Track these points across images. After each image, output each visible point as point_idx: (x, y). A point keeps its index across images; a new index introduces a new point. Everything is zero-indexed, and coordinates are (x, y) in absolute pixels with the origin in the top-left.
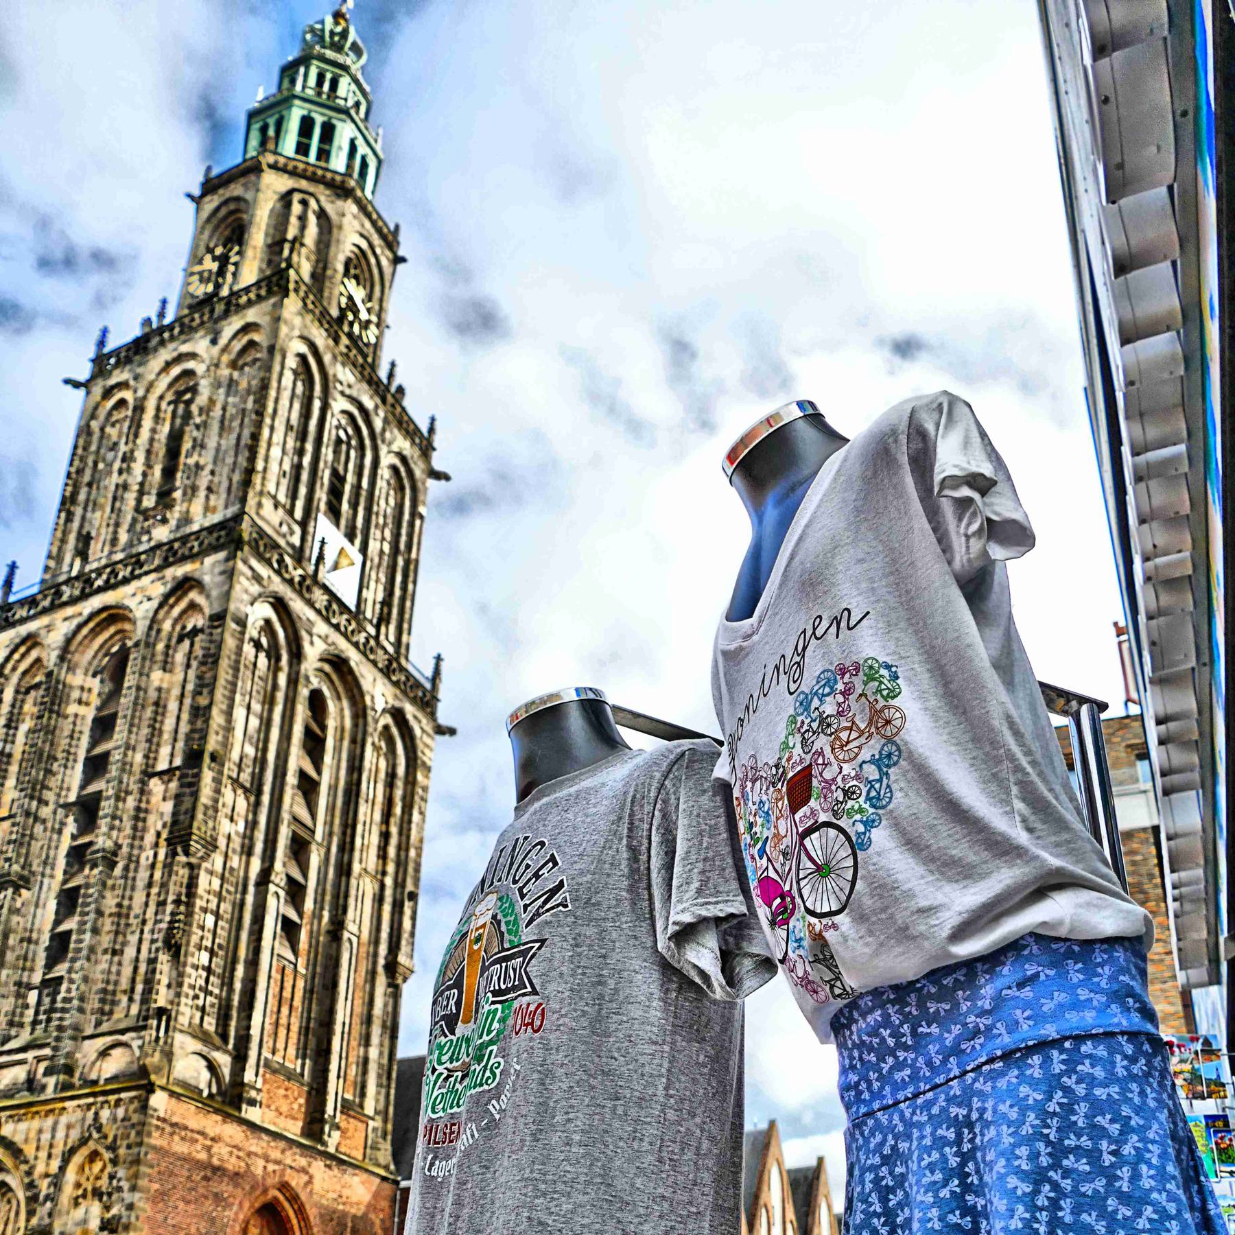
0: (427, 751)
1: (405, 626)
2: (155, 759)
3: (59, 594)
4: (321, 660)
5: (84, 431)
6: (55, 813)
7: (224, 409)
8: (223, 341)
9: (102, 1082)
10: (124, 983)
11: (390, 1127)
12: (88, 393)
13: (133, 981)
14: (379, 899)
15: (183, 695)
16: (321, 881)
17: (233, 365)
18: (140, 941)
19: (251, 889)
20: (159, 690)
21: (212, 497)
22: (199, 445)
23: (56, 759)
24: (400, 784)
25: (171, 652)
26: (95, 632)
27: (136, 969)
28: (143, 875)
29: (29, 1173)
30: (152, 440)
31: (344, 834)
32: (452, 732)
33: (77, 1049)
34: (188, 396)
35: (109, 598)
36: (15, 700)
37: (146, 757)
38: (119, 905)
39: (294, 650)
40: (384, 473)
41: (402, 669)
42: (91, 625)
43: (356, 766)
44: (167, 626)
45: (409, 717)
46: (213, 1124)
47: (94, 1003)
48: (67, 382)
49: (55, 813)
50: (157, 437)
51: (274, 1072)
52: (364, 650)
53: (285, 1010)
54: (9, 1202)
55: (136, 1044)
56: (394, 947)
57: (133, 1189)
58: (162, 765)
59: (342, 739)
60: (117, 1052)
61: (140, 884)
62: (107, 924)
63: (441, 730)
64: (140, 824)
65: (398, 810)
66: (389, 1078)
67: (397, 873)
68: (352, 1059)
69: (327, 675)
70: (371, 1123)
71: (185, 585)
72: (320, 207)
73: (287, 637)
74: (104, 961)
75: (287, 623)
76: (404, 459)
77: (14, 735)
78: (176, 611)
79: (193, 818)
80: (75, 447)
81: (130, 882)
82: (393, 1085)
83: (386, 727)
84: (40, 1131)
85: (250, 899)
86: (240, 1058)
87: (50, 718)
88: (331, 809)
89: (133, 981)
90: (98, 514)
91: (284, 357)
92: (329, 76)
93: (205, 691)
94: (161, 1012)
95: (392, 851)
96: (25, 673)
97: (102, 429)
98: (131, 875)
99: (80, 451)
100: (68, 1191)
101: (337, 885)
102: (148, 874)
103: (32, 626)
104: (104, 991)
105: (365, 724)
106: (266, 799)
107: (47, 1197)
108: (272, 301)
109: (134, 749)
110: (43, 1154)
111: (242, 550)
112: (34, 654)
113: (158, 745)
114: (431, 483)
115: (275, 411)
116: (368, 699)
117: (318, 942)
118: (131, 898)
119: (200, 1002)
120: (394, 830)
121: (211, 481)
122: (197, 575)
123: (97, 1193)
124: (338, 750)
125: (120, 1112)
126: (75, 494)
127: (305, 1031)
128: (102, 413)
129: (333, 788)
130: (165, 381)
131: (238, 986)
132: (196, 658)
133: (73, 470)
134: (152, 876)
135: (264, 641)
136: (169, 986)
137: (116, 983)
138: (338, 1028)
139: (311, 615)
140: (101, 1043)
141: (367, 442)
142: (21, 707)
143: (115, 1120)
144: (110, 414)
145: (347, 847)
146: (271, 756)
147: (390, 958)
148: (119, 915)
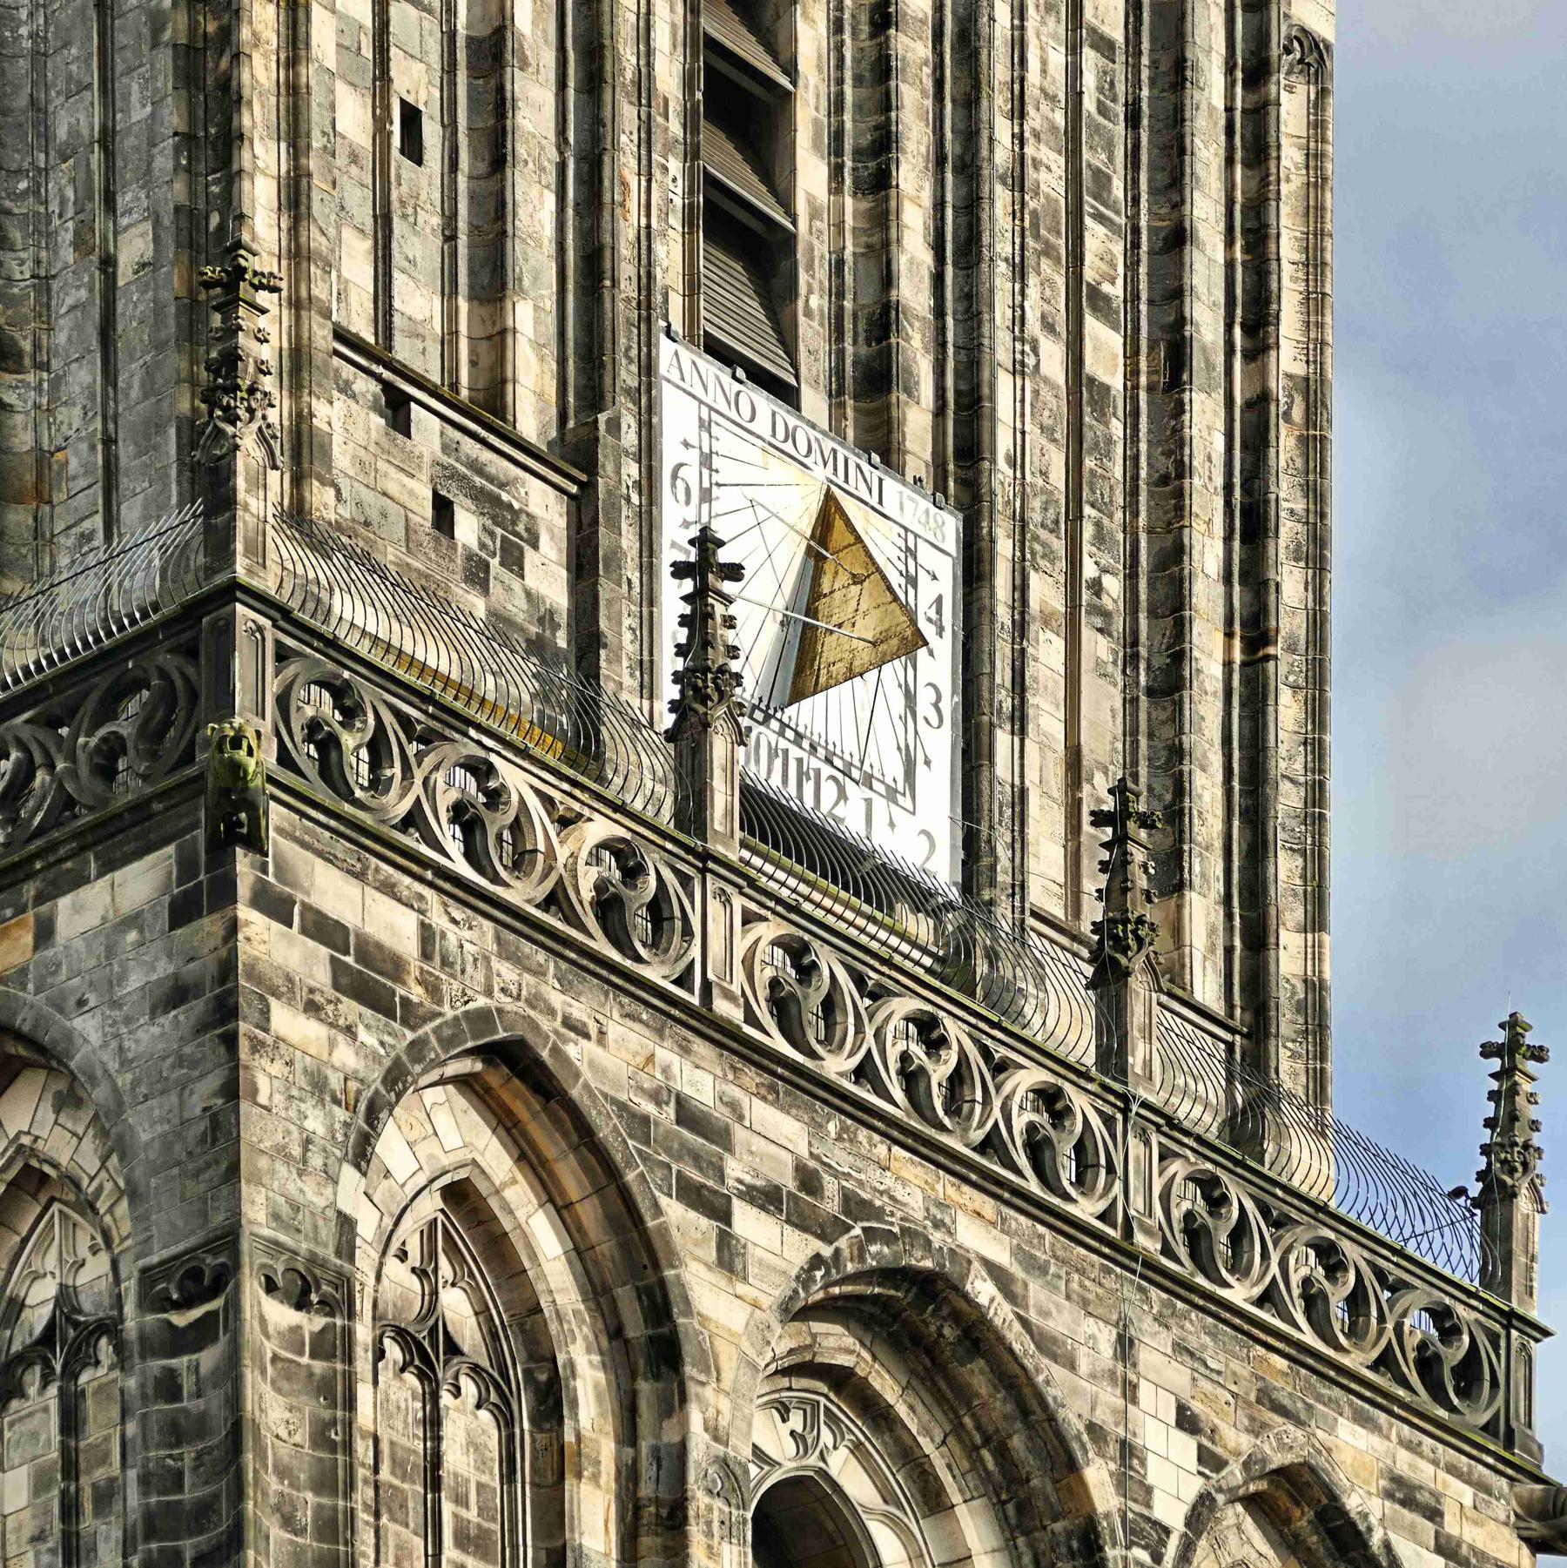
1: (1286, 868)
4: (797, 1312)
39: (635, 1328)
69: (841, 1379)
73: (580, 1252)
111: (255, 843)
116: (1098, 1476)
132: (106, 1496)
135: (456, 1307)
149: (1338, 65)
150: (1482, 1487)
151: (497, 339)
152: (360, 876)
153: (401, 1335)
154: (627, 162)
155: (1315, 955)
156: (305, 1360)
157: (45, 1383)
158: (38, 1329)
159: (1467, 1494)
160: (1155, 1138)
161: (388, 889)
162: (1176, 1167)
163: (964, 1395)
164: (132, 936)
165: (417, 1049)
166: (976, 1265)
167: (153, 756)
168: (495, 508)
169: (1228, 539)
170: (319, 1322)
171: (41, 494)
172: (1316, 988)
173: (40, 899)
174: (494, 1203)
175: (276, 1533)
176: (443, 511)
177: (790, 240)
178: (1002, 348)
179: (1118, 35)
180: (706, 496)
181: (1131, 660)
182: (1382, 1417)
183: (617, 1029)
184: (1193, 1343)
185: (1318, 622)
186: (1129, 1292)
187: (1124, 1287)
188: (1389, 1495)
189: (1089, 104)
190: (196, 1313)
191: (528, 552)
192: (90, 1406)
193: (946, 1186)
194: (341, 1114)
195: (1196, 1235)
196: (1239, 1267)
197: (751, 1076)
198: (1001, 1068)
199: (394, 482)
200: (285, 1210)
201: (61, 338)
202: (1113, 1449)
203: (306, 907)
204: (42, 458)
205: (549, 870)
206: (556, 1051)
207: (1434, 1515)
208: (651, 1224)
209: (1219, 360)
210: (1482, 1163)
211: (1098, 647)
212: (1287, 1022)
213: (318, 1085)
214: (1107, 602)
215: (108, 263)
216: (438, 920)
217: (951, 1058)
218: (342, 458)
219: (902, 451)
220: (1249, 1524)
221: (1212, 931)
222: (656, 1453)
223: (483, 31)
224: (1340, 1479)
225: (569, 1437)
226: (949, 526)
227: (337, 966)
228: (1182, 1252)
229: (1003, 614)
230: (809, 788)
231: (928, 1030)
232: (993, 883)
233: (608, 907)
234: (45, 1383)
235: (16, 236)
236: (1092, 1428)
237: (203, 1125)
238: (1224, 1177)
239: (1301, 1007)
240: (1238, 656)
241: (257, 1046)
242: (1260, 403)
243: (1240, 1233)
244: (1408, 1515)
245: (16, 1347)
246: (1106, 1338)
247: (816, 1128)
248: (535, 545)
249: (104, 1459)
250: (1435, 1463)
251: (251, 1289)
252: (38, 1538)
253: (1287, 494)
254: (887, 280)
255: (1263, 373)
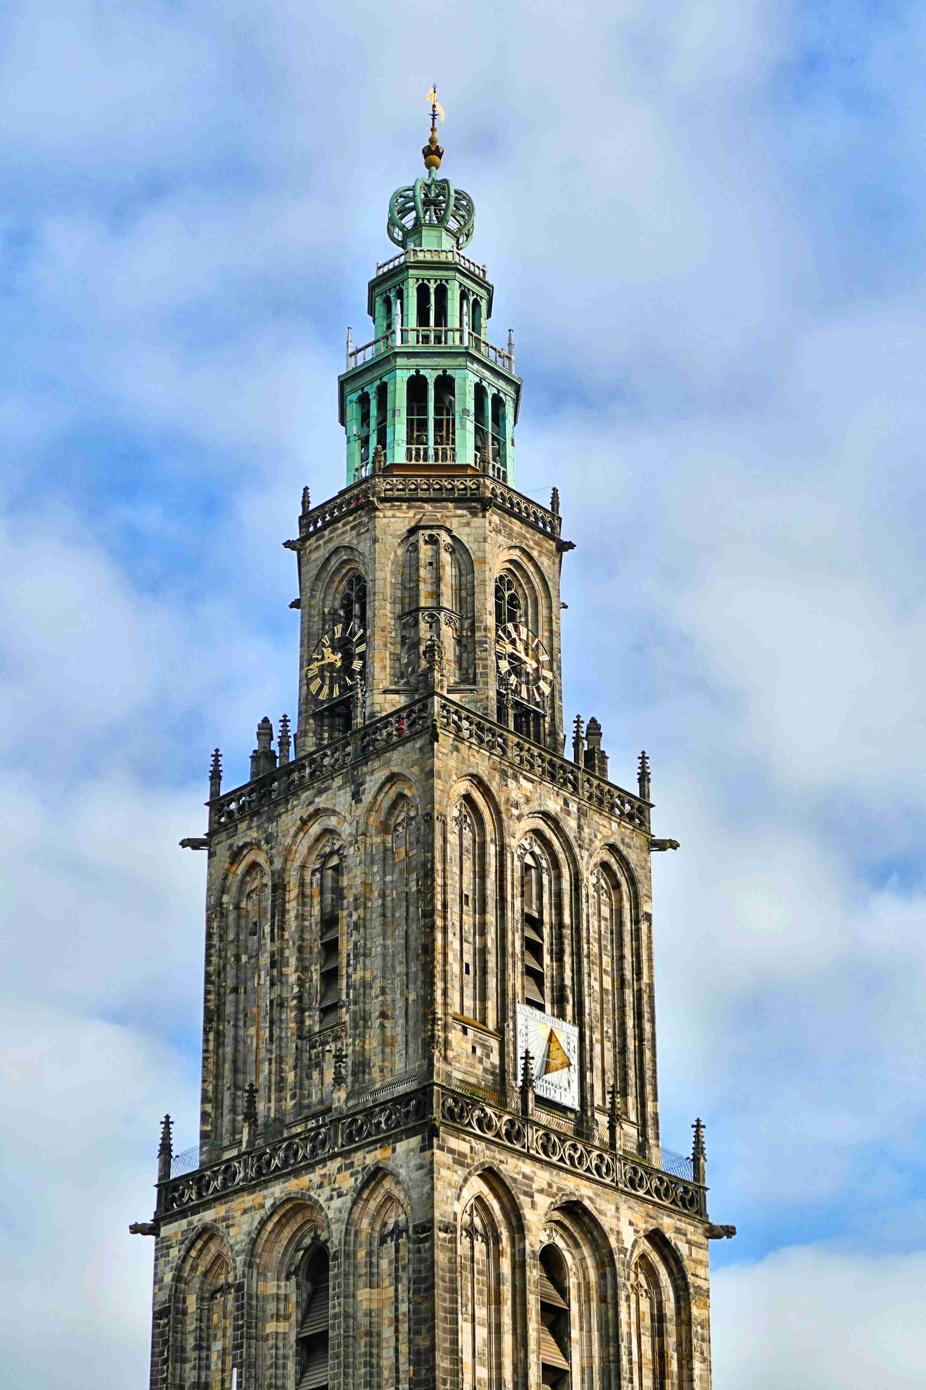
0: (701, 1271)
1: (649, 1088)
5: (215, 910)
7: (383, 896)
8: (367, 798)
12: (211, 855)
17: (385, 828)
20: (369, 1313)
21: (388, 1024)
22: (360, 953)
24: (671, 1327)
25: (374, 1260)
30: (302, 930)
32: (729, 1231)
34: (335, 861)
35: (293, 1185)
36: (201, 1309)
39: (514, 1223)
44: (365, 1224)
59: (588, 1300)
63: (713, 1233)
71: (376, 1175)
73: (503, 1208)
75: (500, 1191)
77: (208, 1358)
78: (372, 1205)
80: (209, 936)
83: (643, 1256)
87: (249, 1347)
91: (444, 824)
92: (432, 286)
93: (424, 1328)
96: (206, 1274)
97: (237, 907)
103: (209, 1216)
105: (615, 1275)
111: (438, 1136)
112: (213, 1248)
114: (656, 856)
116: (612, 1240)
121: (383, 1004)
122: (391, 1165)
124: (585, 1315)
126: (221, 1004)
130: (304, 843)
135: (477, 1221)
141: (562, 856)
142: (209, 1319)
144: (243, 882)
149: (654, 918)
150: (696, 1227)
151: (484, 1009)
152: (458, 1138)
153: (466, 1230)
154: (510, 971)
155: (655, 1107)
156: (447, 1244)
157: (392, 1241)
158: (391, 1229)
159: (692, 1229)
160: (622, 1162)
161: (464, 1140)
162: (627, 1167)
163: (584, 1223)
164: (412, 1153)
165: (470, 1174)
166: (585, 1198)
167: (417, 1115)
168: (484, 1046)
169: (634, 1019)
170: (450, 1236)
171: (392, 1045)
172: (656, 1114)
173: (393, 1143)
174: (485, 1200)
175: (441, 1283)
176: (474, 1049)
177: (542, 974)
178: (586, 991)
179: (608, 917)
180: (527, 1035)
181: (615, 1046)
182: (673, 1215)
183: (510, 1160)
184: (632, 1206)
185: (653, 1035)
186: (618, 1197)
187: (616, 1195)
188: (675, 1232)
189: (603, 932)
190: (425, 1235)
191: (491, 1054)
192: (401, 1247)
194: (454, 1190)
195: (632, 1181)
196: (641, 1186)
197: (538, 1165)
198: (589, 1152)
199: (464, 1045)
200: (443, 1213)
201: (397, 1013)
202: (615, 1233)
203: (448, 1147)
204: (393, 1037)
205: (496, 1128)
206: (498, 1168)
207: (685, 1235)
208: (517, 1202)
209: (631, 982)
210: (693, 1151)
211: (608, 1045)
212: (650, 1122)
213: (450, 1184)
214: (609, 1035)
215: (407, 999)
216: (474, 1144)
217: (579, 1152)
218: (454, 1043)
219: (566, 1015)
220: (645, 1241)
221: (633, 1104)
222: (519, 1250)
223: (481, 947)
224: (665, 1230)
225: (501, 1248)
227: (454, 1158)
228: (629, 1186)
229: (588, 1047)
230: (548, 1092)
231: (574, 1147)
232: (587, 1105)
233: (508, 1133)
234: (392, 1241)
235: (388, 992)
236: (611, 1229)
237: (426, 1196)
238: (637, 1167)
239: (653, 1119)
240: (637, 1044)
241: (438, 1179)
242: (640, 990)
243: (641, 1178)
244: (680, 1236)
245: (385, 1233)
246: (613, 1208)
247: (551, 1173)
248: (492, 1052)
249: (404, 1259)
250: (685, 1223)
251: (436, 1230)
252: (390, 1275)
253: (646, 1009)
254: (563, 979)
255: (640, 985)
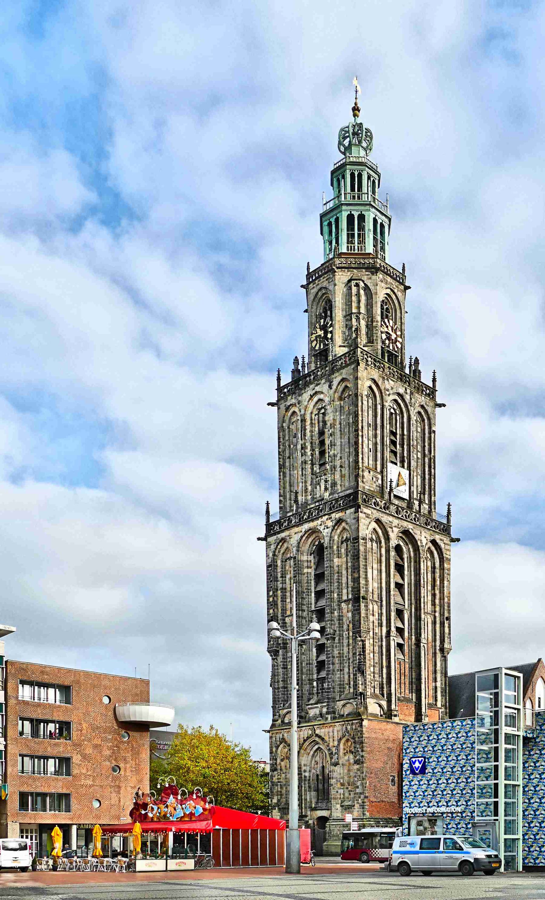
0: (448, 553)
1: (433, 492)
2: (342, 595)
3: (290, 521)
6: (308, 614)
7: (340, 424)
8: (334, 387)
9: (345, 715)
10: (346, 681)
11: (448, 711)
13: (349, 680)
14: (434, 623)
15: (347, 568)
16: (410, 624)
17: (341, 399)
18: (349, 666)
19: (384, 639)
20: (338, 566)
21: (343, 469)
23: (304, 592)
25: (339, 549)
26: (308, 538)
27: (349, 676)
28: (345, 642)
29: (328, 746)
30: (312, 436)
31: (416, 603)
33: (335, 705)
34: (323, 411)
35: (311, 525)
37: (338, 595)
38: (339, 653)
40: (414, 417)
41: (433, 520)
42: (306, 535)
43: (418, 573)
44: (336, 538)
45: (438, 541)
46: (384, 725)
47: (337, 689)
48: (269, 404)
49: (308, 614)
50: (313, 434)
51: (402, 701)
52: (414, 521)
53: (403, 678)
54: (322, 753)
55: (354, 703)
56: (442, 641)
57: (362, 751)
58: (345, 598)
59: (410, 562)
60: (348, 705)
61: (345, 644)
62: (337, 660)
63: (453, 540)
64: (341, 622)
65: (438, 583)
66: (446, 692)
67: (440, 610)
68: (431, 688)
70: (440, 710)
72: (365, 284)
73: (382, 532)
74: (338, 675)
76: (422, 407)
78: (339, 531)
79: (360, 623)
81: (341, 644)
82: (447, 695)
83: (429, 548)
84: (329, 732)
85: (384, 644)
86: (389, 702)
87: (299, 577)
88: (410, 594)
89: (349, 680)
90: (296, 472)
91: (362, 397)
94: (361, 694)
95: (437, 601)
96: (283, 554)
97: (289, 428)
98: (341, 641)
99: (281, 440)
100: (342, 752)
101: (416, 624)
102: (347, 641)
103: (283, 535)
104: (340, 684)
105: (419, 554)
106: (384, 603)
107: (336, 753)
108: (353, 366)
109: (333, 592)
110: (331, 740)
112: (285, 545)
113: (342, 589)
114: (438, 409)
115: (362, 427)
116: (419, 543)
117: (412, 649)
118: (343, 650)
119: (373, 685)
120: (437, 592)
122: (344, 518)
123: (351, 752)
124: (409, 567)
125: (354, 727)
126: (284, 463)
127: (411, 683)
128: (287, 419)
129: (410, 584)
131: (385, 676)
132: (349, 551)
133: (280, 450)
134: (349, 642)
135: (374, 537)
136: (362, 684)
137: (343, 681)
138: (423, 681)
139: (391, 519)
140: (342, 702)
141: (404, 409)
143: (352, 729)
144: (290, 419)
145: (418, 609)
146: (384, 585)
147: (441, 646)
148: (340, 657)
151: (376, 465)
154: (385, 451)
168: (376, 477)
185: (435, 474)
187: (421, 528)
193: (408, 523)
199: (369, 477)
211: (419, 477)
212: (433, 504)
218: (366, 476)
226: (408, 472)
231: (407, 512)
233: (384, 508)
253: (432, 464)
